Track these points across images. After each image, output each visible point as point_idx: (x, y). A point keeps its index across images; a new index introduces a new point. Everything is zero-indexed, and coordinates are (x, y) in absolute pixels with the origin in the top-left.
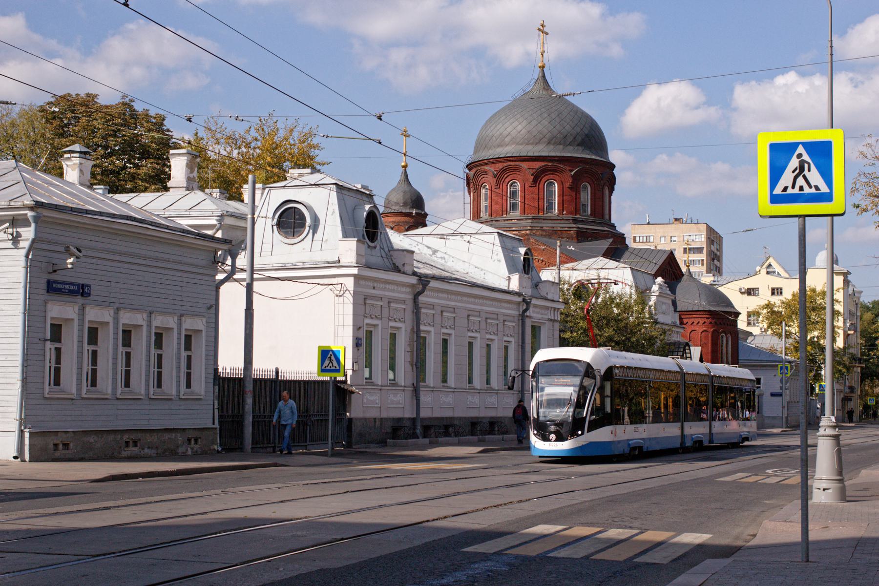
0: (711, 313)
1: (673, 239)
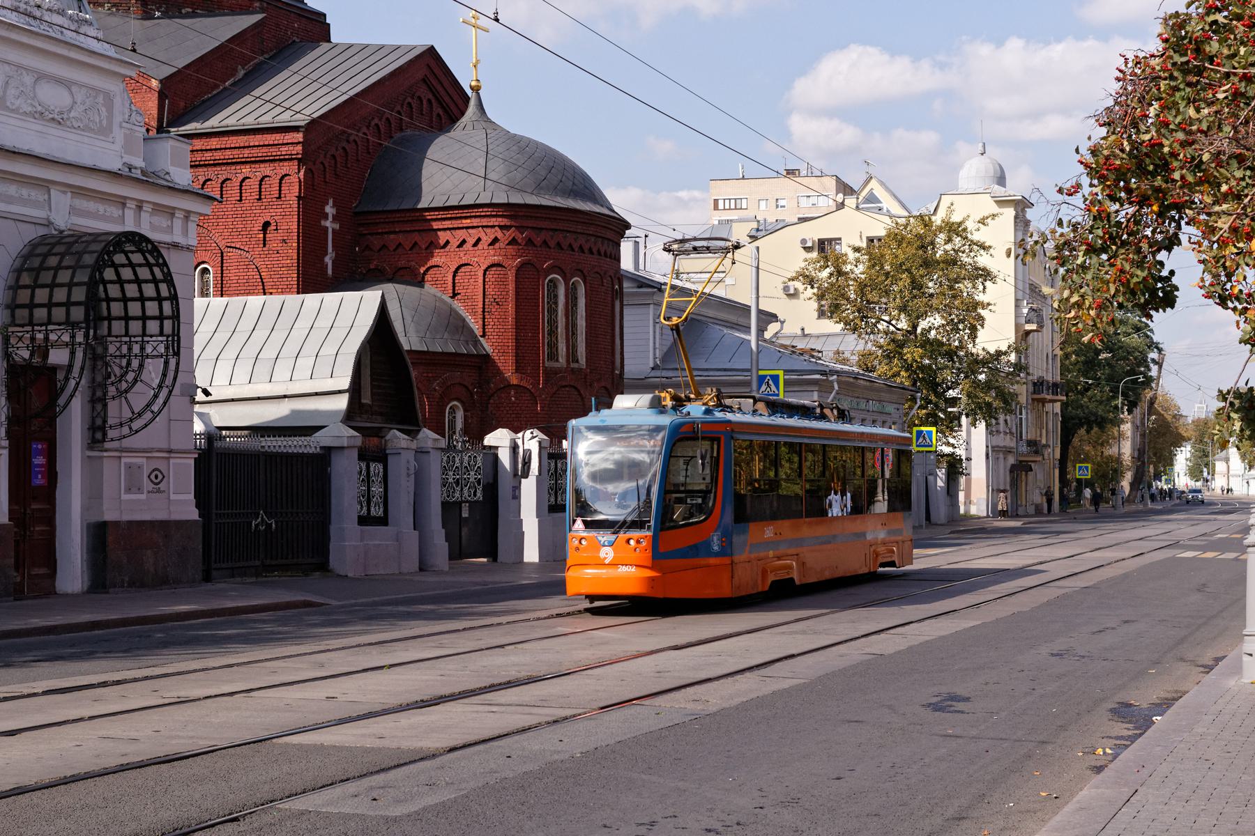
0: (510, 210)
1: (781, 203)
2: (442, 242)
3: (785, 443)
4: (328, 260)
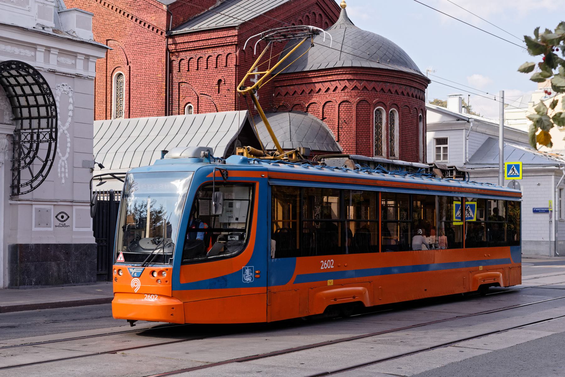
2: (317, 89)
3: (438, 196)
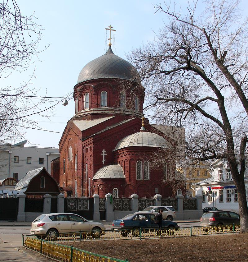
4: (104, 161)
